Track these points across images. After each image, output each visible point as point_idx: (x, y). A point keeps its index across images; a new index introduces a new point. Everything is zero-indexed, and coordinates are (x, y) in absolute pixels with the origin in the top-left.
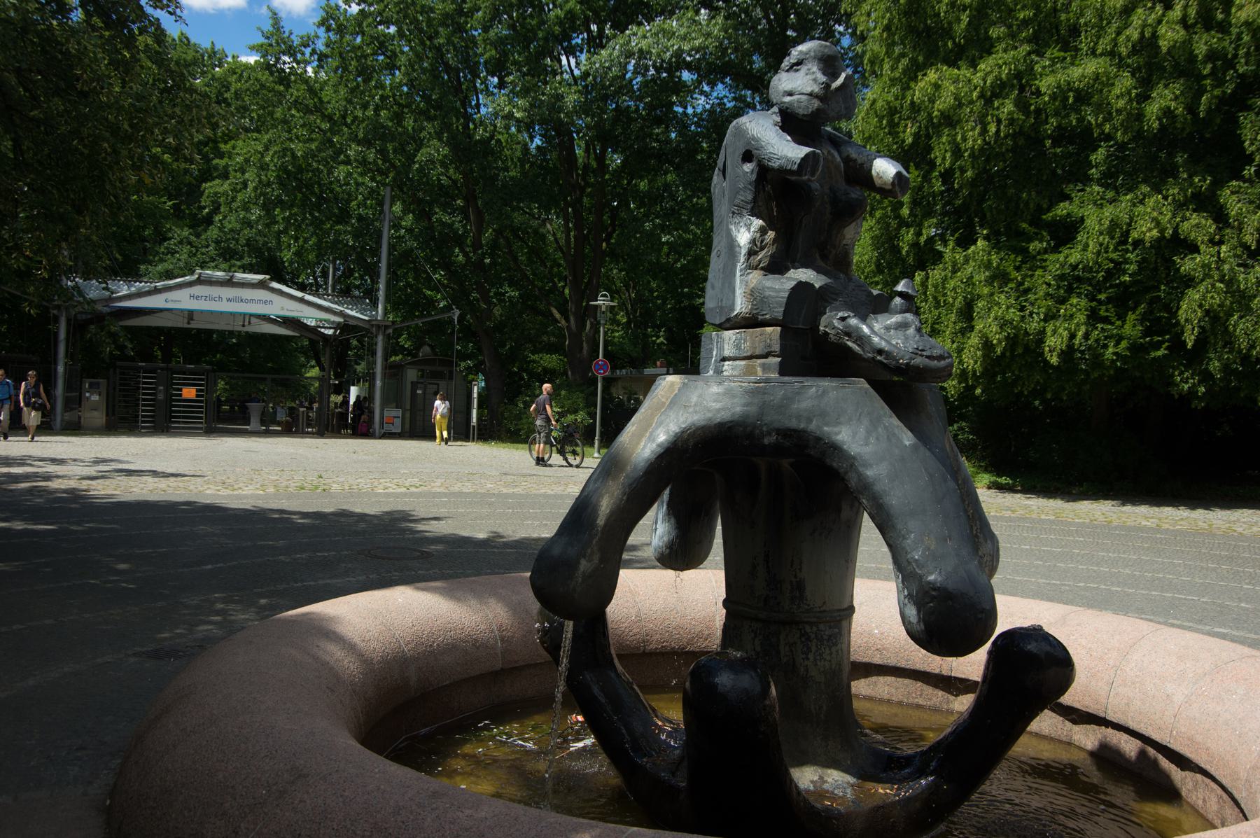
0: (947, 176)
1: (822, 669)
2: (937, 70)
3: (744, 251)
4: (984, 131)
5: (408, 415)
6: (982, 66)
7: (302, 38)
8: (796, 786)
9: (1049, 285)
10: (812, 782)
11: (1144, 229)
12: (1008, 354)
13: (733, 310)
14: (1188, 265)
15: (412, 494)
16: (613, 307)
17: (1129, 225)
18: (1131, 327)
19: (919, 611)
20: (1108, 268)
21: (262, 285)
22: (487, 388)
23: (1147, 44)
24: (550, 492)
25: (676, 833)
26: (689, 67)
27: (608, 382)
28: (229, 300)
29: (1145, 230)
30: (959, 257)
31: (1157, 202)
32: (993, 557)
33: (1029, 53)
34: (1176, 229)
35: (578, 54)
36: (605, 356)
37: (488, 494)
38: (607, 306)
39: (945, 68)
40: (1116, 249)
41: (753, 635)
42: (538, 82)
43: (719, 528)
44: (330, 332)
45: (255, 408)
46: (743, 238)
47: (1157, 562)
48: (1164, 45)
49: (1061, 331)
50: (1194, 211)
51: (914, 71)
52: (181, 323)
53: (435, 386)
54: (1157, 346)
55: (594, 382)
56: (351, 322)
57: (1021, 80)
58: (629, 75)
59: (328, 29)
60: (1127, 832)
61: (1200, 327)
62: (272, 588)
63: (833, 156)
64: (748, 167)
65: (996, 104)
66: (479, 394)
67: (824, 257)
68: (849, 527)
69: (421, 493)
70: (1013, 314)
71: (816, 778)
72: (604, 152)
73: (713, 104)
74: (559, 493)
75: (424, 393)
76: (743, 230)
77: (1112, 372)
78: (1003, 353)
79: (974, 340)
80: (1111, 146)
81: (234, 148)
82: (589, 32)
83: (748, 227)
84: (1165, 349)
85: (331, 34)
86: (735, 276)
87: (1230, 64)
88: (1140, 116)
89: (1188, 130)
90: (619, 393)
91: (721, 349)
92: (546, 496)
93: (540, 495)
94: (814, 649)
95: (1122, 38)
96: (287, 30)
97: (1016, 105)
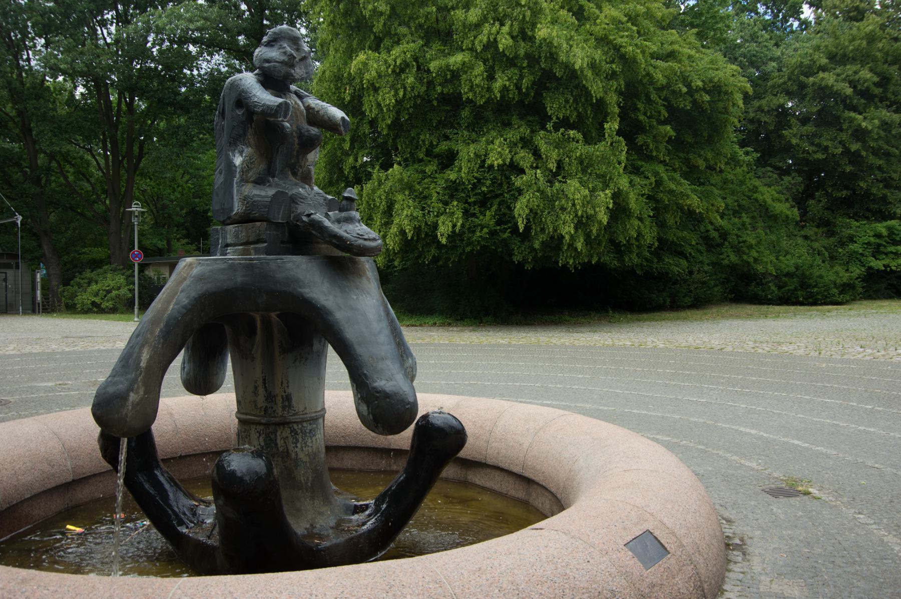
3: (238, 170)
4: (396, 94)
8: (295, 533)
9: (438, 193)
10: (306, 529)
11: (494, 159)
12: (415, 238)
13: (232, 211)
14: (518, 182)
16: (143, 213)
17: (485, 156)
18: (488, 218)
22: (48, 274)
23: (492, 45)
24: (102, 348)
25: (384, 562)
26: (195, 42)
27: (142, 267)
29: (494, 160)
30: (383, 175)
31: (500, 143)
33: (423, 46)
34: (512, 159)
35: (109, 26)
36: (139, 248)
37: (54, 353)
39: (370, 52)
40: (478, 171)
41: (258, 434)
42: (110, 59)
43: (229, 364)
46: (238, 160)
48: (501, 47)
49: (447, 222)
51: (350, 54)
53: (4, 275)
54: (505, 230)
55: (132, 267)
58: (149, 45)
60: (537, 529)
61: (527, 219)
63: (299, 106)
64: (240, 112)
65: (403, 77)
66: (42, 279)
67: (294, 174)
68: (319, 356)
70: (418, 213)
71: (308, 526)
72: (132, 100)
73: (213, 69)
74: (110, 348)
76: (237, 155)
77: (478, 248)
78: (412, 238)
79: (394, 229)
82: (117, 11)
83: (241, 153)
86: (233, 187)
87: (538, 61)
88: (489, 89)
89: (517, 99)
90: (150, 273)
91: (225, 238)
92: (99, 351)
93: (96, 351)
94: (300, 440)
97: (415, 79)
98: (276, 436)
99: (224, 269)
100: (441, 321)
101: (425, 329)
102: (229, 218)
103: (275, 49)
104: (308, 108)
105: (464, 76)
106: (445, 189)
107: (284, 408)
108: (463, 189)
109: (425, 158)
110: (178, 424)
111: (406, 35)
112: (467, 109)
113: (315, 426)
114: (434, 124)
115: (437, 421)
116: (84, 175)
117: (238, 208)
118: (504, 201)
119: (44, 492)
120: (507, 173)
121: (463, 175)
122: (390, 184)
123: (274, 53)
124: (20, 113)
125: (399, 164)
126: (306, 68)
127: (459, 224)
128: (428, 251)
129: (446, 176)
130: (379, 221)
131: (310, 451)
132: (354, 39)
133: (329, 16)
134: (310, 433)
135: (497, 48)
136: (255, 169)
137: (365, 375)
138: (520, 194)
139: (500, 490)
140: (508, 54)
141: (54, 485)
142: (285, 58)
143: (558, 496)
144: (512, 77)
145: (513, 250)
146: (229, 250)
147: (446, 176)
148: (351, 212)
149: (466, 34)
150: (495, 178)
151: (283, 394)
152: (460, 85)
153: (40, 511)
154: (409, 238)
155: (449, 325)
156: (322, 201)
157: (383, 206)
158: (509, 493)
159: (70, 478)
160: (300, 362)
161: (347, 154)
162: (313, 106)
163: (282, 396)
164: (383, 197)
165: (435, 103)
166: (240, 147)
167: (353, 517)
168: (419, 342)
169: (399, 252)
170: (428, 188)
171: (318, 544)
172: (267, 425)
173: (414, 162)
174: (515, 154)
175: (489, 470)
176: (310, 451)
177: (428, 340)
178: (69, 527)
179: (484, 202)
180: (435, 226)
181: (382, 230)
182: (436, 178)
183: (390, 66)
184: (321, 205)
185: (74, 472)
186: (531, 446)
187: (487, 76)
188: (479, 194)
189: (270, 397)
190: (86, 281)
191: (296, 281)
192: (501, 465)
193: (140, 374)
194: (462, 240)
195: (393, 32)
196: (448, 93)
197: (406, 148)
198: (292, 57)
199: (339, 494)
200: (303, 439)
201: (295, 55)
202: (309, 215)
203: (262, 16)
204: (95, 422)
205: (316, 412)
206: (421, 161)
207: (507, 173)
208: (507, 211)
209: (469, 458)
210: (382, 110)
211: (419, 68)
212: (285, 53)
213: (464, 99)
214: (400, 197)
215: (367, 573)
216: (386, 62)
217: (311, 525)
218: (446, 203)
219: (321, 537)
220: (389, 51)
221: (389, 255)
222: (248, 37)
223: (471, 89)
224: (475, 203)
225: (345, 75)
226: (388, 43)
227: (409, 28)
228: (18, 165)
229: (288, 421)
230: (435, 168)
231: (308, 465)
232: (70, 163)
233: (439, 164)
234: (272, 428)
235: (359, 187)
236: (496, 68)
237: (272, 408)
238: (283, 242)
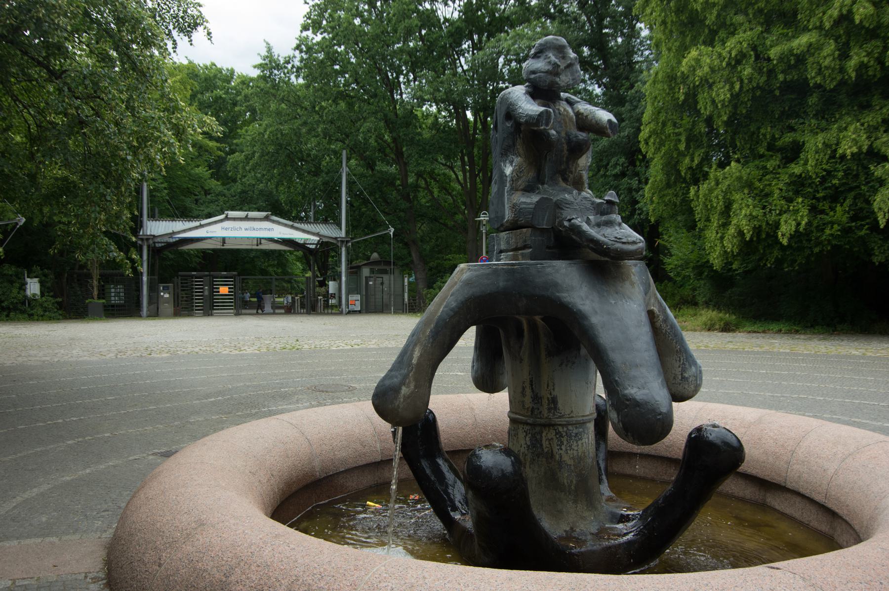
0: (709, 121)
1: (571, 456)
2: (698, 48)
3: (508, 179)
4: (732, 87)
5: (364, 297)
6: (728, 44)
7: (285, 58)
9: (781, 190)
10: (565, 531)
11: (846, 147)
12: (755, 239)
13: (504, 219)
15: (353, 350)
18: (841, 213)
19: (618, 415)
20: (823, 176)
21: (266, 218)
28: (246, 229)
29: (847, 148)
31: (856, 128)
32: (696, 377)
33: (762, 32)
39: (703, 47)
40: (827, 163)
41: (525, 434)
45: (268, 299)
46: (508, 170)
47: (855, 379)
48: (857, 19)
49: (790, 221)
50: (885, 132)
51: (683, 50)
52: (219, 246)
54: (860, 228)
56: (325, 240)
57: (759, 53)
59: (301, 51)
62: (249, 412)
63: (567, 112)
64: (509, 124)
65: (739, 69)
67: (565, 180)
69: (360, 349)
70: (758, 212)
71: (568, 529)
75: (375, 284)
76: (508, 165)
77: (829, 248)
78: (751, 239)
79: (732, 230)
81: (247, 131)
83: (511, 163)
84: (866, 230)
85: (303, 54)
88: (842, 70)
89: (879, 76)
91: (499, 244)
94: (565, 443)
95: (825, 18)
97: (754, 69)
98: (541, 436)
99: (488, 274)
100: (788, 328)
101: (768, 336)
102: (502, 225)
103: (541, 59)
104: (578, 114)
105: (811, 60)
106: (788, 184)
107: (549, 409)
108: (810, 184)
109: (766, 153)
110: (477, 419)
111: (743, 24)
112: (815, 95)
113: (581, 430)
114: (777, 116)
115: (712, 436)
116: (445, 189)
117: (508, 215)
118: (860, 194)
119: (356, 468)
120: (865, 162)
121: (810, 168)
122: (727, 183)
123: (539, 64)
124: (394, 140)
125: (738, 161)
126: (572, 74)
127: (804, 223)
128: (771, 253)
129: (790, 171)
130: (716, 222)
131: (575, 454)
132: (688, 35)
133: (660, 15)
134: (575, 437)
135: (852, 21)
136: (524, 177)
137: (616, 381)
138: (881, 186)
139: (801, 519)
140: (867, 25)
141: (364, 462)
142: (549, 67)
143: (861, 535)
144: (872, 51)
145: (873, 249)
146: (503, 255)
147: (790, 171)
148: (611, 215)
149: (814, 11)
150: (849, 169)
151: (549, 396)
152: (806, 70)
153: (354, 483)
154: (747, 239)
155: (797, 332)
156: (589, 205)
157: (720, 206)
158: (811, 524)
159: (379, 459)
160: (566, 366)
161: (682, 154)
162: (582, 111)
163: (548, 399)
164: (720, 197)
165: (777, 93)
166: (511, 157)
167: (617, 526)
168: (756, 349)
169: (738, 254)
170: (770, 185)
171: (572, 548)
172: (533, 425)
173: (754, 159)
174: (875, 140)
175: (789, 495)
176: (575, 454)
177: (767, 348)
178: (368, 503)
179: (835, 197)
180: (777, 225)
181: (719, 231)
182: (779, 173)
183: (724, 59)
184: (588, 209)
185: (382, 453)
186: (836, 473)
187: (839, 55)
188: (830, 188)
189: (537, 398)
191: (555, 285)
192: (801, 490)
193: (412, 370)
194: (809, 240)
195: (728, 23)
196: (792, 81)
197: (746, 144)
198: (556, 66)
199: (614, 501)
200: (568, 442)
201: (559, 63)
202: (570, 220)
203: (601, 26)
204: (373, 409)
205: (584, 416)
206: (762, 156)
207: (865, 162)
208: (864, 205)
209: (767, 478)
210: (717, 106)
211: (757, 57)
212: (550, 62)
213: (811, 85)
214: (737, 196)
215: (558, 583)
216: (720, 55)
217: (572, 528)
218: (790, 200)
219: (579, 542)
220: (724, 43)
221: (727, 258)
222: (591, 48)
223: (820, 72)
224: (824, 198)
225: (679, 74)
226: (723, 35)
227: (747, 15)
228: (392, 184)
229: (553, 423)
230: (778, 163)
231: (572, 467)
232: (435, 180)
233: (783, 158)
234: (538, 429)
235: (696, 187)
236: (852, 44)
237: (538, 409)
238: (548, 247)
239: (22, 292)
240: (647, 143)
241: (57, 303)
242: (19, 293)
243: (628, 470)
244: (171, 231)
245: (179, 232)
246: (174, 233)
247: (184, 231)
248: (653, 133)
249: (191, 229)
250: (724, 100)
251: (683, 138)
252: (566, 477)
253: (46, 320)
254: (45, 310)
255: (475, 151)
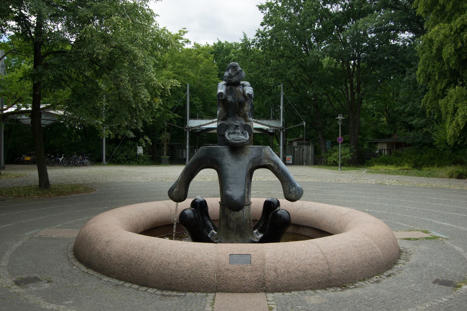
38: (341, 119)
44: (272, 131)
59: (259, 37)
65: (462, 34)
67: (239, 116)
80: (285, 14)
96: (248, 38)
190: (333, 151)
239: (135, 152)
240: (420, 77)
241: (150, 157)
242: (134, 153)
243: (303, 233)
244: (200, 125)
245: (203, 125)
246: (201, 125)
247: (205, 125)
248: (422, 71)
249: (208, 124)
250: (450, 53)
251: (437, 73)
252: (231, 225)
253: (145, 165)
254: (145, 160)
255: (354, 80)
